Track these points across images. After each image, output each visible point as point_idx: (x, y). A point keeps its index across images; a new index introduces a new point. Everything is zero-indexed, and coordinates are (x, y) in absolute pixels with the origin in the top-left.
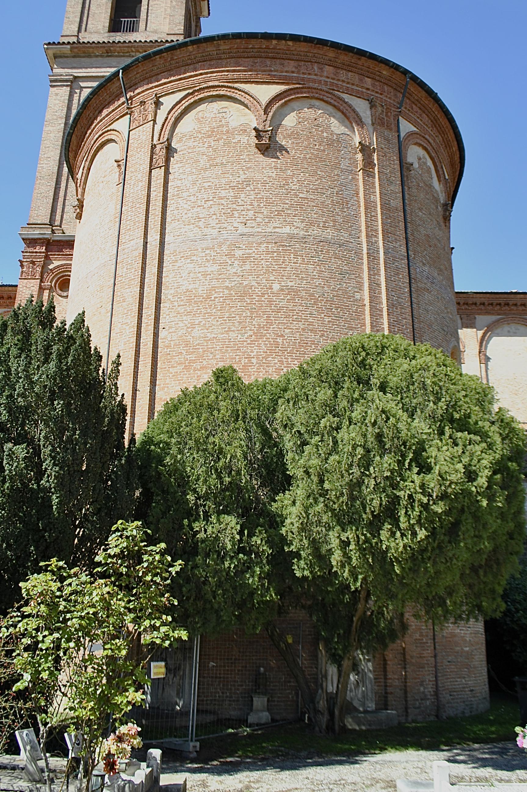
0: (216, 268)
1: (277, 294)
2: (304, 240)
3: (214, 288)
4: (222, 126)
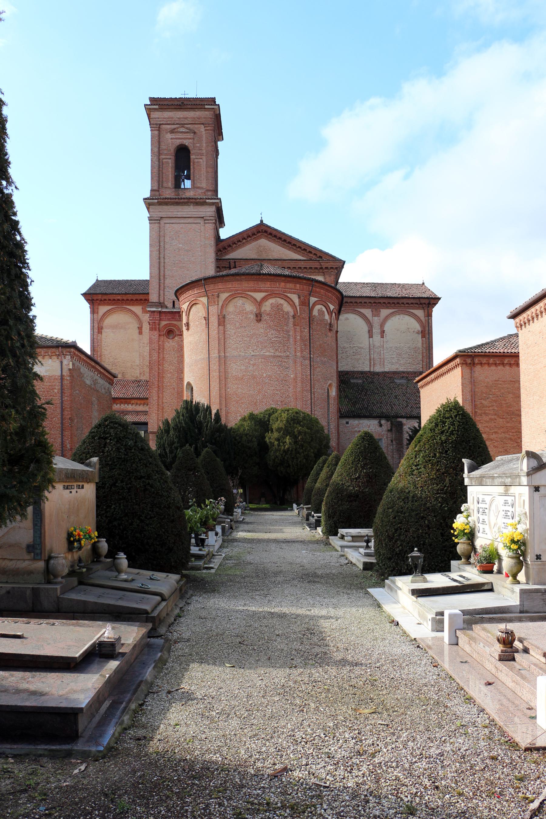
0: (244, 368)
1: (265, 378)
2: (274, 357)
3: (244, 375)
4: (244, 310)
